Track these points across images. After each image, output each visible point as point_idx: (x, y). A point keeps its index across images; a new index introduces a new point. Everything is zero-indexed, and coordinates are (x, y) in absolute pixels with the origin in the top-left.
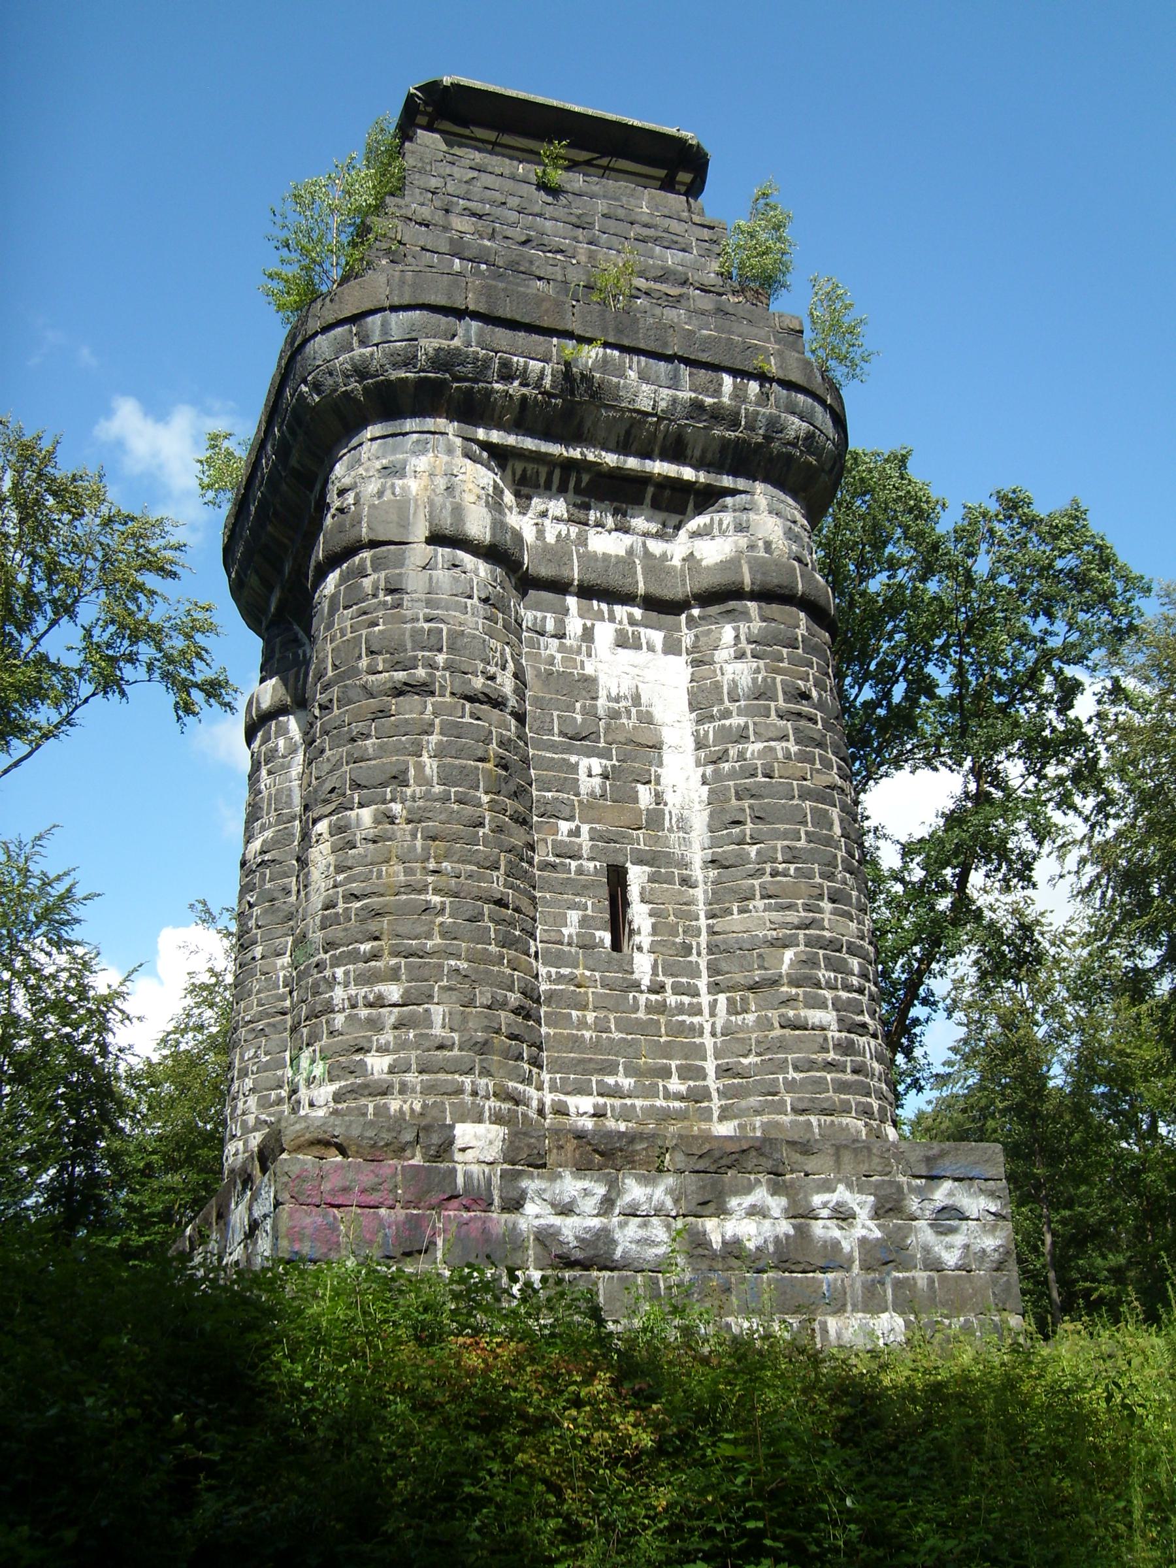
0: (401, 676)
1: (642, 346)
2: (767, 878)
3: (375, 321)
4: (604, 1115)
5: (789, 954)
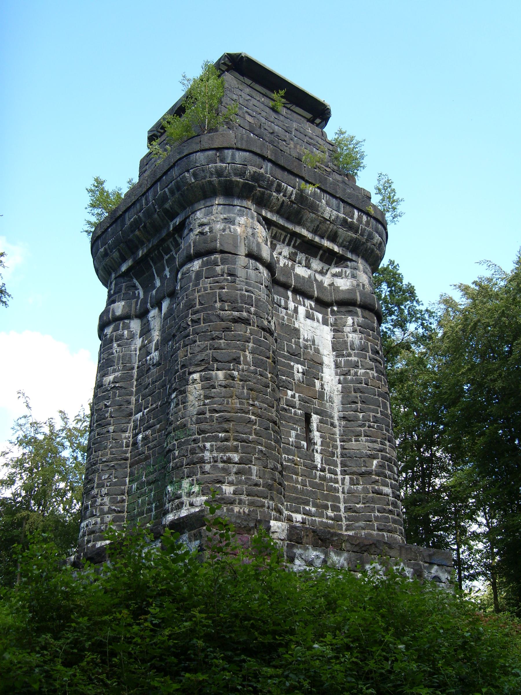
0: (236, 314)
1: (328, 190)
2: (366, 428)
3: (228, 153)
4: (305, 523)
5: (375, 462)
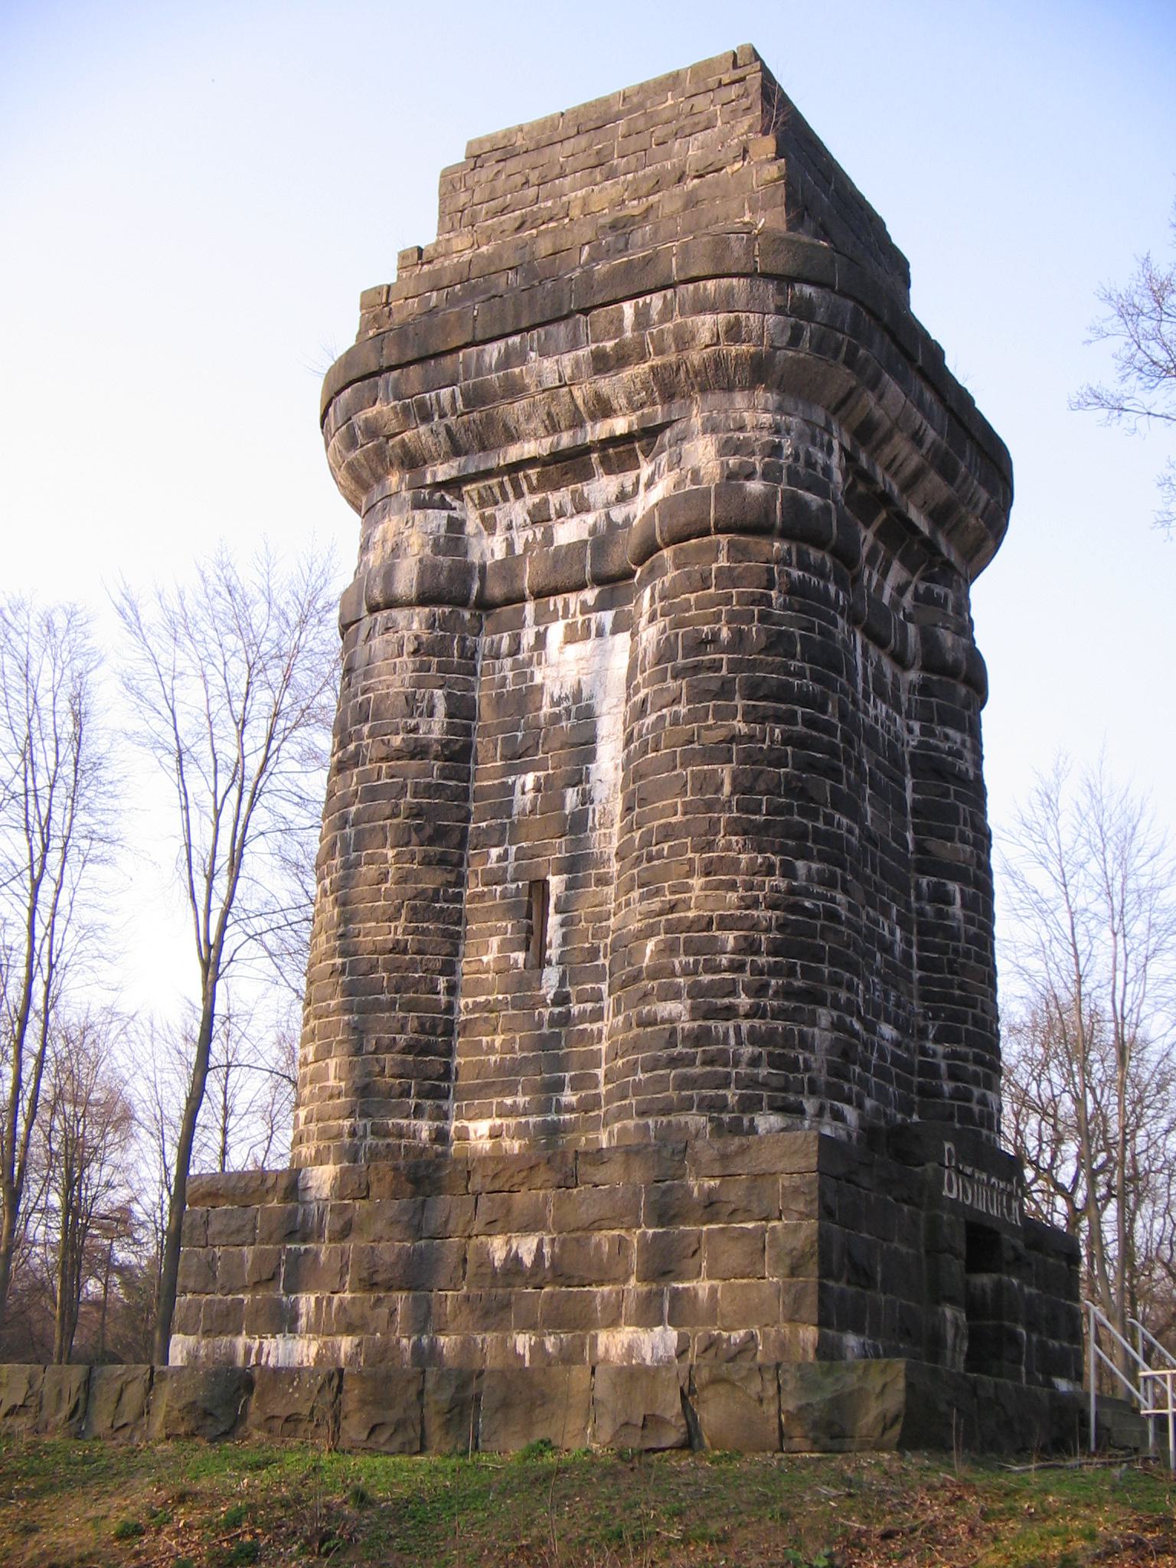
5: (650, 945)
